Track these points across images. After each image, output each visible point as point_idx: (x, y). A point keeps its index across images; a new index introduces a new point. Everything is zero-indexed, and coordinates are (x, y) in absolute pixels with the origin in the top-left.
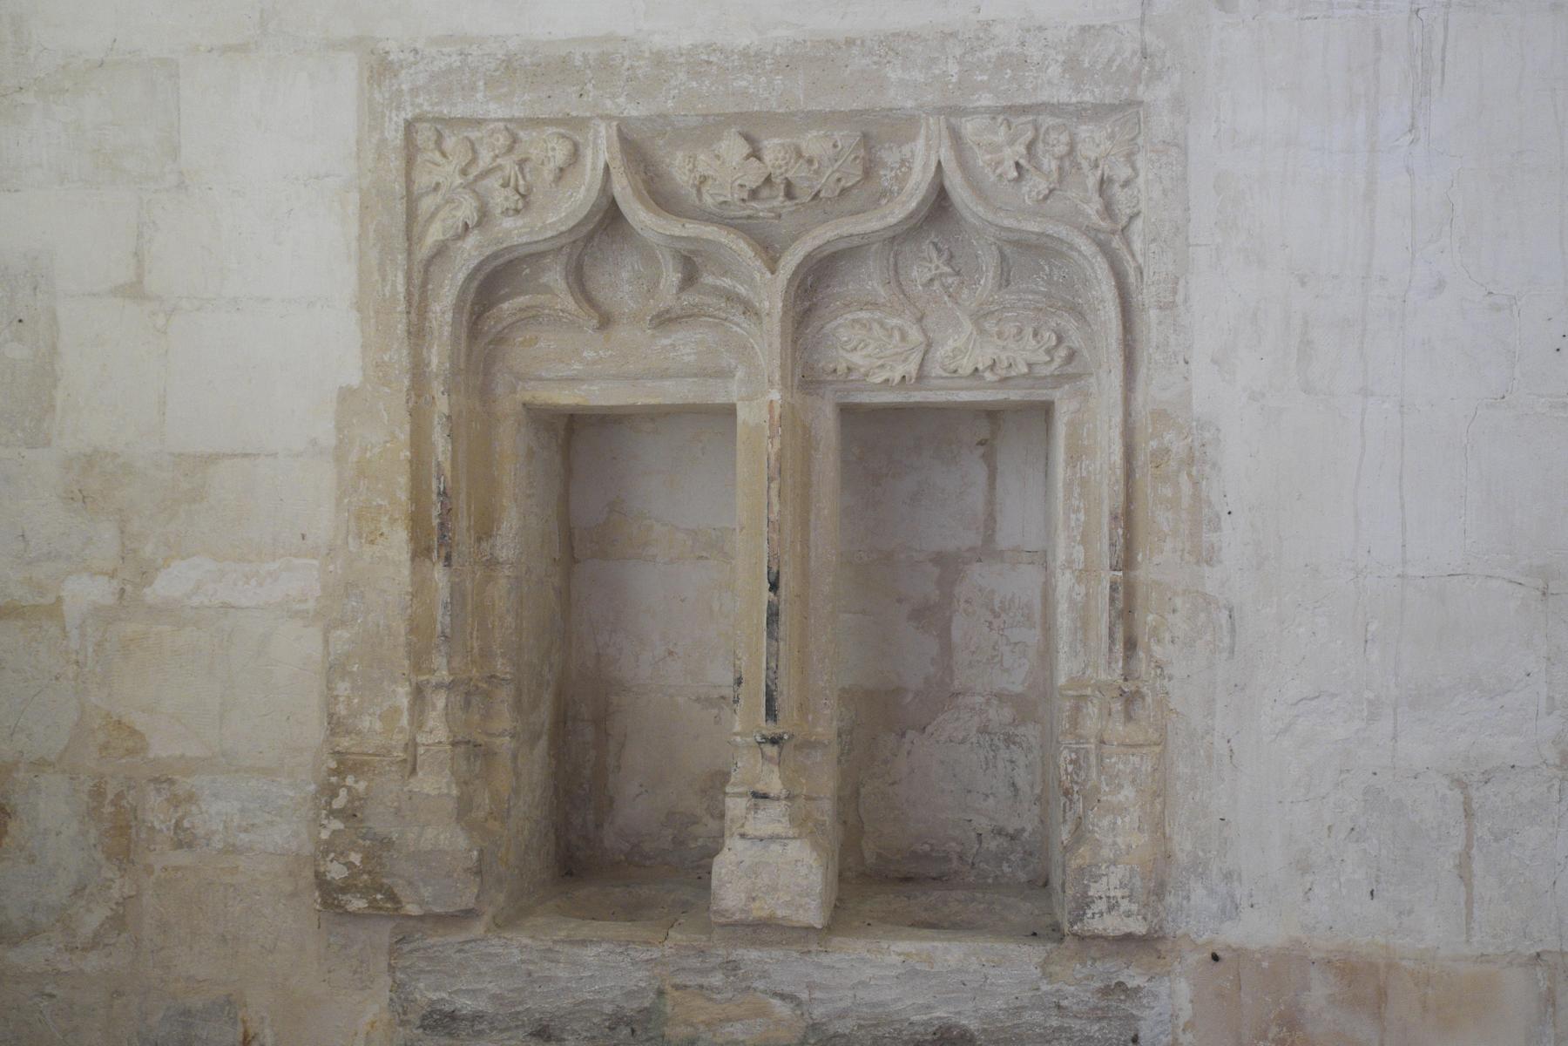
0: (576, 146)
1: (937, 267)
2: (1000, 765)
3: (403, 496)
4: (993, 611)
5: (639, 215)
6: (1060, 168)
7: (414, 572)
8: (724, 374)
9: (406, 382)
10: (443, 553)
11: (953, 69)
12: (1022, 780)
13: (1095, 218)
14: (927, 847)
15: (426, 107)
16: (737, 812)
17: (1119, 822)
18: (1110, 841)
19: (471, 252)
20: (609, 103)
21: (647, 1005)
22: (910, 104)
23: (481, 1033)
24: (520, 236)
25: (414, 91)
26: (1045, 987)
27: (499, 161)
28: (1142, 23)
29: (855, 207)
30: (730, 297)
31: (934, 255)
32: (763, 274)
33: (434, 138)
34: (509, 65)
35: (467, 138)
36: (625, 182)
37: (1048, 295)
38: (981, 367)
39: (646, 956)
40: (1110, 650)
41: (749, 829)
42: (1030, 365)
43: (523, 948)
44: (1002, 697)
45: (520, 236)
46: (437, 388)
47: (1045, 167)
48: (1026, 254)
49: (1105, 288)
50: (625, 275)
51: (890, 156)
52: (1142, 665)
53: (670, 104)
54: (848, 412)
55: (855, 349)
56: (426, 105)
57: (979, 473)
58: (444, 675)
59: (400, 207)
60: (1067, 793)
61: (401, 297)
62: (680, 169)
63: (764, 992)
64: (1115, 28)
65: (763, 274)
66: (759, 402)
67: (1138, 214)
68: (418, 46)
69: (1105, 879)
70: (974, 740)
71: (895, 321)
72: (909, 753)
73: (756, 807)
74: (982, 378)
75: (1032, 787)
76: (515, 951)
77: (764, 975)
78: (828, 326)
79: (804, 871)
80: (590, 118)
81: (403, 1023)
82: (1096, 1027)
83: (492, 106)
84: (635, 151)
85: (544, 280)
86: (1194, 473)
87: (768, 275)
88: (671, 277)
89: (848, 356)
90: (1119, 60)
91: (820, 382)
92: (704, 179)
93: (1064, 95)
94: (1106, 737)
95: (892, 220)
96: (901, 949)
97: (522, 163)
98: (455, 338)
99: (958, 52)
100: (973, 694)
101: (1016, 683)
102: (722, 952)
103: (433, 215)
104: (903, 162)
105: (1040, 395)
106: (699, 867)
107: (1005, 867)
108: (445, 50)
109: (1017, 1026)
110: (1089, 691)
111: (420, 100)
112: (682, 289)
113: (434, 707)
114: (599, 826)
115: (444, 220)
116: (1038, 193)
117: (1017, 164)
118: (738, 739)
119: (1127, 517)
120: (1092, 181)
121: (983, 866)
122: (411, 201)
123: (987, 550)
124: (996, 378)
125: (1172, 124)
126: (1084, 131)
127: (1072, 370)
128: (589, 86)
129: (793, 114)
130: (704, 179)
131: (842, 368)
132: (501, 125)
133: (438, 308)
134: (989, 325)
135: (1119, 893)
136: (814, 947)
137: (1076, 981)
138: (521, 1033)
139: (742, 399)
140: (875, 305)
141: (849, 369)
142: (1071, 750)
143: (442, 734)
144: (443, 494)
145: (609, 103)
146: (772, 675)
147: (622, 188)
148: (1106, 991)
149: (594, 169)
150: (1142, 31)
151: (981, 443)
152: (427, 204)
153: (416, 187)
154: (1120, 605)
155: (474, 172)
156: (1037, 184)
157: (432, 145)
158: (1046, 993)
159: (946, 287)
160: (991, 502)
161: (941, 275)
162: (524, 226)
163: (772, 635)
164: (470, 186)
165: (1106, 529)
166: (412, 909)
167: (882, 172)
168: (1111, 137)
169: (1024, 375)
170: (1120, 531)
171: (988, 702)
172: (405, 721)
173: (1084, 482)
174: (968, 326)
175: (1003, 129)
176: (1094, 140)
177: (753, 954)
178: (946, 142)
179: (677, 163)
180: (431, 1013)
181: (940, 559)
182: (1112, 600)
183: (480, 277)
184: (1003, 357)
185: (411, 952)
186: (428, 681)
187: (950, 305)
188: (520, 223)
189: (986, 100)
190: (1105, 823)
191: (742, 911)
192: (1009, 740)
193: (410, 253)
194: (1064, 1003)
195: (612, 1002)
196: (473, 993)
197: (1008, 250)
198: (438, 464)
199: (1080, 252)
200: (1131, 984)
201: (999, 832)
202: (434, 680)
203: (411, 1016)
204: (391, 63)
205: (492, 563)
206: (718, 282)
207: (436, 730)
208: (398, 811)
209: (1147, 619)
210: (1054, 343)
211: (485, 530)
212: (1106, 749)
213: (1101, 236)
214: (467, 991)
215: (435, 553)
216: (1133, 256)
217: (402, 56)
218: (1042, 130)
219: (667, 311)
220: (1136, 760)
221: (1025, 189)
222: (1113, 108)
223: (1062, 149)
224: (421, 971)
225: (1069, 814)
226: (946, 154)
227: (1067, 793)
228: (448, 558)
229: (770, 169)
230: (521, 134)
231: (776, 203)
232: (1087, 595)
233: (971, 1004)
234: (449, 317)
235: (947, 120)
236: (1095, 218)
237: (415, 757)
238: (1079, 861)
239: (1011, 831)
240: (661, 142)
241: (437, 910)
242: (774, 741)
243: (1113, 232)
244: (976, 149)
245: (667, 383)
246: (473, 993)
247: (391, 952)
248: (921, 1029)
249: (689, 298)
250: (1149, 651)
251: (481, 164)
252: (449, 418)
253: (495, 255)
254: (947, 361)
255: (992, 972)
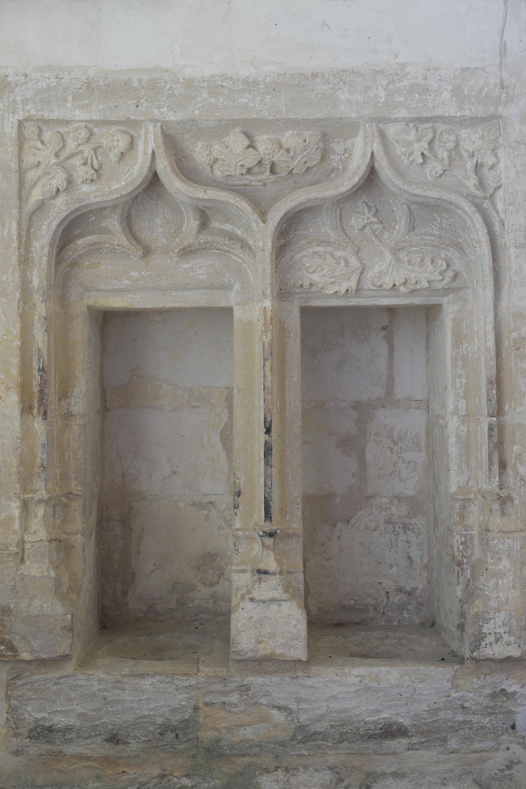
0: (132, 138)
1: (368, 218)
2: (400, 544)
3: (15, 372)
4: (393, 441)
5: (173, 183)
6: (450, 157)
7: (22, 424)
8: (227, 287)
9: (18, 295)
10: (42, 411)
11: (382, 93)
12: (415, 553)
13: (473, 189)
14: (352, 602)
15: (33, 112)
16: (240, 583)
17: (500, 583)
18: (494, 596)
19: (60, 209)
20: (156, 112)
21: (187, 717)
22: (354, 115)
23: (70, 740)
24: (95, 197)
25: (25, 102)
26: (454, 695)
27: (81, 147)
28: (501, 66)
29: (315, 176)
30: (232, 237)
31: (366, 210)
32: (258, 224)
33: (37, 132)
34: (89, 86)
35: (59, 132)
36: (166, 162)
37: (440, 237)
38: (397, 283)
39: (186, 684)
40: (490, 469)
41: (255, 594)
42: (429, 282)
43: (100, 680)
44: (400, 498)
45: (95, 197)
46: (37, 298)
47: (440, 155)
48: (425, 210)
49: (480, 234)
50: (159, 221)
51: (338, 147)
52: (511, 479)
53: (197, 112)
54: (307, 312)
55: (315, 271)
56: (32, 110)
57: (382, 348)
58: (43, 494)
59: (15, 178)
60: (459, 564)
61: (15, 237)
62: (199, 153)
63: (267, 705)
64: (484, 69)
65: (258, 224)
66: (253, 308)
67: (500, 187)
68: (28, 72)
69: (493, 621)
70: (382, 528)
71: (339, 253)
72: (339, 538)
73: (260, 580)
74: (398, 290)
75: (422, 558)
76: (95, 683)
77: (267, 694)
78: (296, 257)
79: (294, 622)
80: (144, 121)
81: (16, 735)
82: (487, 720)
83: (78, 112)
84: (172, 143)
85: (104, 224)
86: (53, 166)
87: (262, 224)
88: (192, 223)
89: (310, 276)
90: (486, 89)
91: (289, 293)
92: (216, 160)
93: (452, 111)
94: (490, 527)
95: (343, 189)
96: (358, 673)
97: (95, 150)
98: (49, 264)
99: (384, 83)
100: (381, 497)
101: (409, 488)
102: (239, 679)
103: (35, 183)
104: (346, 150)
105: (433, 300)
106: (195, 620)
107: (406, 615)
108: (47, 75)
109: (436, 721)
110: (472, 496)
111: (29, 107)
112: (199, 231)
113: (36, 515)
114: (125, 594)
115: (43, 186)
116: (436, 173)
117: (423, 154)
118: (240, 533)
119: (498, 382)
120: (470, 165)
121: (390, 613)
122: (21, 173)
123: (389, 400)
124: (407, 290)
125: (521, 130)
126: (464, 133)
127: (456, 286)
128: (143, 100)
129: (278, 120)
130: (216, 160)
131: (306, 283)
132: (83, 124)
133: (38, 245)
134: (402, 256)
135: (502, 630)
136: (300, 674)
137: (474, 690)
138: (99, 740)
139: (238, 304)
140: (328, 243)
141: (311, 284)
142: (461, 535)
143: (42, 534)
144: (42, 370)
145: (156, 112)
146: (268, 490)
147: (164, 167)
148: (494, 696)
149: (145, 154)
150: (500, 72)
151: (384, 328)
152: (31, 175)
153: (24, 164)
154: (495, 439)
155: (64, 155)
156: (435, 167)
157: (35, 137)
158: (454, 698)
159: (374, 231)
160: (390, 367)
161: (371, 223)
162: (95, 191)
163: (268, 463)
164: (61, 164)
165: (484, 390)
166: (26, 656)
167: (332, 157)
168: (482, 138)
169: (426, 289)
170: (494, 391)
171: (391, 502)
172: (16, 526)
173: (464, 358)
174: (389, 257)
175: (413, 132)
176: (471, 139)
177: (259, 680)
178: (377, 139)
179: (197, 149)
180: (35, 728)
181: (357, 406)
182: (490, 437)
183: (65, 224)
184: (412, 276)
185: (22, 685)
186: (32, 498)
187: (376, 243)
188: (94, 188)
189: (403, 113)
190: (491, 583)
191: (252, 651)
192: (406, 527)
193: (20, 208)
194: (466, 705)
195: (162, 716)
196: (65, 713)
197: (413, 207)
198: (39, 350)
199: (464, 211)
200: (510, 690)
201: (401, 590)
202: (37, 497)
203: (20, 730)
204: (9, 83)
205: (68, 415)
206: (222, 227)
207: (39, 532)
208: (14, 587)
209: (514, 449)
210: (445, 268)
211: (64, 394)
212: (490, 534)
213: (476, 201)
214: (61, 712)
215: (35, 411)
216: (497, 213)
217: (17, 78)
218: (438, 133)
219: (189, 246)
220: (511, 541)
221: (427, 170)
222: (483, 120)
223: (450, 145)
224: (29, 699)
225: (461, 578)
226: (377, 147)
227: (459, 564)
228: (45, 413)
229: (262, 155)
230: (95, 130)
231: (264, 177)
232: (468, 432)
233: (405, 708)
234: (46, 250)
235: (377, 126)
236: (473, 189)
237: (23, 551)
238: (476, 610)
239: (408, 589)
240: (188, 136)
241: (43, 656)
242: (271, 535)
243: (485, 198)
244: (396, 144)
245: (187, 293)
246: (65, 713)
247: (8, 687)
248: (372, 727)
249: (204, 238)
250: (515, 469)
251: (68, 149)
252: (45, 318)
253: (77, 210)
254: (376, 280)
255: (420, 686)
